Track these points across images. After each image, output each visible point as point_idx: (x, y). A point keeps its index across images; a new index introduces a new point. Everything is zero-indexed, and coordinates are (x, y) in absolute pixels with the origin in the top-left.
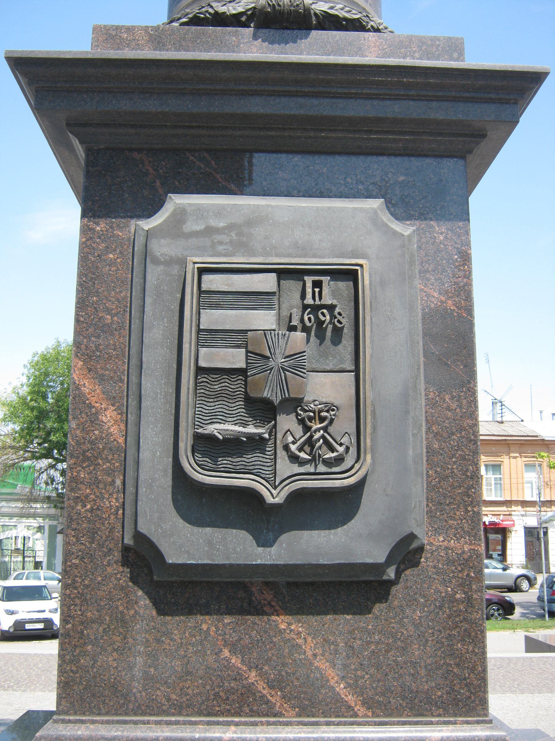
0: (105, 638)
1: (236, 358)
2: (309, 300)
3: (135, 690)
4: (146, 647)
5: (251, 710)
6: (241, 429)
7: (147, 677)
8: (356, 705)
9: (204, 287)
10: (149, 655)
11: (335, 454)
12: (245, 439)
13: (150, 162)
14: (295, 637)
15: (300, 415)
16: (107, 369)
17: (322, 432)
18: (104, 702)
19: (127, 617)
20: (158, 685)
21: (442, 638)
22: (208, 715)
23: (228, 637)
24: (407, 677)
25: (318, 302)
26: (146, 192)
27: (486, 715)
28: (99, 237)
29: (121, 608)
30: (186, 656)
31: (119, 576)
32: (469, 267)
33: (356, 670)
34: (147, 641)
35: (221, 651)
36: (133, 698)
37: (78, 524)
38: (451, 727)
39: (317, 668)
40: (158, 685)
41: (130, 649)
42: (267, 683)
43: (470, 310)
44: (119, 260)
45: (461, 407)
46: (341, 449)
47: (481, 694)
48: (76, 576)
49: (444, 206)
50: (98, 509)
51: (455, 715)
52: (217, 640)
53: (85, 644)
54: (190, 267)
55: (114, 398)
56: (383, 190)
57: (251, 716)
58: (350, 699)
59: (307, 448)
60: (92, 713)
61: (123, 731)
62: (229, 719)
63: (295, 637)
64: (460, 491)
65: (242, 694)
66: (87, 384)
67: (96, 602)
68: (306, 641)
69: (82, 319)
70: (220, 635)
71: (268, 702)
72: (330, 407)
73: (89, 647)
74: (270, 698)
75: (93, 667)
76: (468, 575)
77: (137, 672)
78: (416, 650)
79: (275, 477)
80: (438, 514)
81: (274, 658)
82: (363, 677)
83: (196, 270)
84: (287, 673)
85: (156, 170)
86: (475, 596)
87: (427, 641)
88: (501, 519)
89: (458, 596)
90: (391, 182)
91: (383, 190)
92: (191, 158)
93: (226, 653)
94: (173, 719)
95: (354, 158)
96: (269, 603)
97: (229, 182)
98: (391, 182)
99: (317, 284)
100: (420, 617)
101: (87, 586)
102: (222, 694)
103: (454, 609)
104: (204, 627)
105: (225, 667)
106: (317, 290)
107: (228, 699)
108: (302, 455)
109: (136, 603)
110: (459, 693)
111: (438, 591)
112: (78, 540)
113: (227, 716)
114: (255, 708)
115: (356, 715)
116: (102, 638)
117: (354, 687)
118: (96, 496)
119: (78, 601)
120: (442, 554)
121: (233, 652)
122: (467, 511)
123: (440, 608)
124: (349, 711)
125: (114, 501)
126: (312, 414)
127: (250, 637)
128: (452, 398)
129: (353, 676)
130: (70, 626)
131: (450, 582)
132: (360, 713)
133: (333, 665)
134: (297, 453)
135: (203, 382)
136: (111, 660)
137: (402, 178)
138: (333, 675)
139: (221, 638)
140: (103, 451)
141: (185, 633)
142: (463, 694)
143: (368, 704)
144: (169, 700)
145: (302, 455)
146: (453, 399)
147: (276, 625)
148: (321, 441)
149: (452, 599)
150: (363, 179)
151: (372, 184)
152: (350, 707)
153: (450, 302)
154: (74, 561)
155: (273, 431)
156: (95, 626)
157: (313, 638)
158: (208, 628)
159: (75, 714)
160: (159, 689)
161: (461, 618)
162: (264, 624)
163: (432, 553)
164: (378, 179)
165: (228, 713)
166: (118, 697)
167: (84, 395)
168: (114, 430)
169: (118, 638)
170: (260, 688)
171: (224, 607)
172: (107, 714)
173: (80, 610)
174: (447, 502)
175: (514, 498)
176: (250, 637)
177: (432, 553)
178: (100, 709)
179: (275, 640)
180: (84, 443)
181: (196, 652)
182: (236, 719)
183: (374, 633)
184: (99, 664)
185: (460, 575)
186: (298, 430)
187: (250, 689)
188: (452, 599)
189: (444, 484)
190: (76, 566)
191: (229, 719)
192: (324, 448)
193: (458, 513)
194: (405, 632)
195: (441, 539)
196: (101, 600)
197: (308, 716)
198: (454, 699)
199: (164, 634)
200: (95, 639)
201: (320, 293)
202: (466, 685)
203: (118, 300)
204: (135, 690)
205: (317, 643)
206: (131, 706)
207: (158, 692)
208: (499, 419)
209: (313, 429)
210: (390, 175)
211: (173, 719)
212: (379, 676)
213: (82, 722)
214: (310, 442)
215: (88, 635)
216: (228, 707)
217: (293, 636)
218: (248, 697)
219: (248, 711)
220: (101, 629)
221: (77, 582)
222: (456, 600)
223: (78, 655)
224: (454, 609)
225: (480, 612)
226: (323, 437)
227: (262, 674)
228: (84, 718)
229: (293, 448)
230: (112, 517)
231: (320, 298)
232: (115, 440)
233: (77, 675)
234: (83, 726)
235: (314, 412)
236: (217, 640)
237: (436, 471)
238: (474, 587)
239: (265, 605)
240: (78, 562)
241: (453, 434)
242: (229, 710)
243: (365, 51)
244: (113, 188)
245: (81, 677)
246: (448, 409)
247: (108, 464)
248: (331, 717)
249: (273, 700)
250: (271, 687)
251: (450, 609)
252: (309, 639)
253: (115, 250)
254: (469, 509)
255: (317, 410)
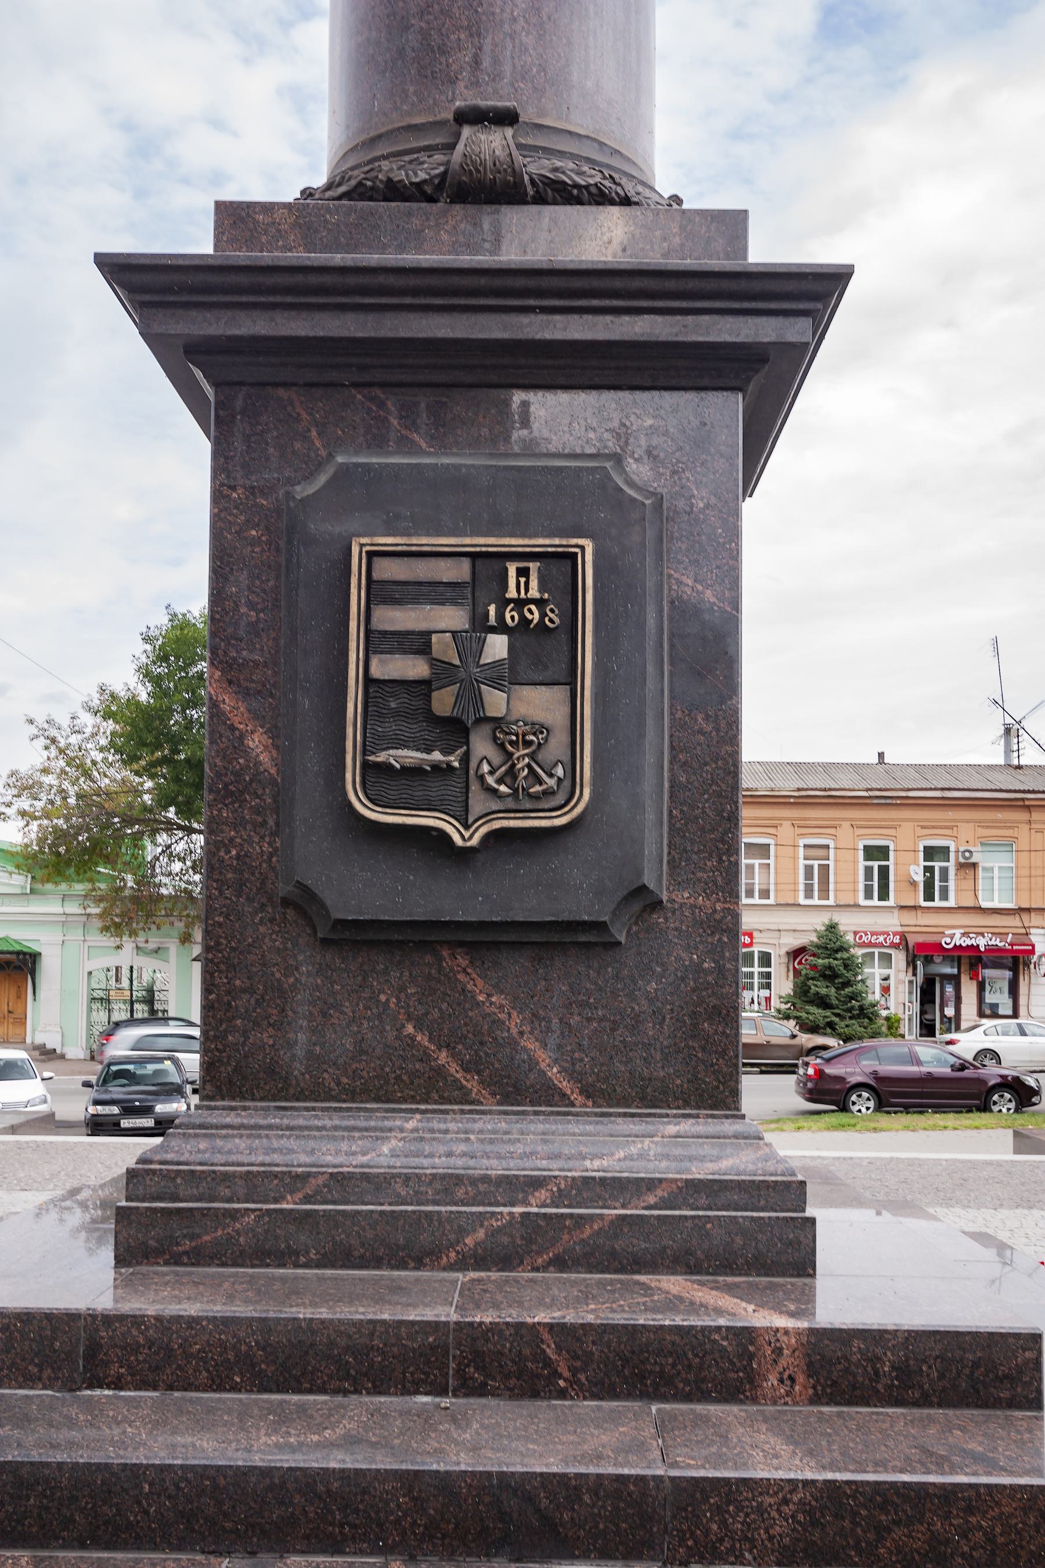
0: (258, 1010)
1: (415, 668)
2: (512, 593)
3: (296, 1073)
4: (309, 1021)
5: (441, 1097)
6: (424, 756)
7: (310, 1055)
8: (572, 1093)
9: (376, 576)
10: (313, 1031)
11: (544, 787)
12: (429, 768)
13: (302, 403)
14: (496, 1011)
15: (499, 739)
16: (253, 681)
17: (527, 760)
18: (258, 1087)
19: (286, 986)
20: (325, 1067)
21: (684, 1015)
22: (388, 1101)
23: (412, 1010)
24: (638, 1061)
25: (523, 595)
26: (297, 445)
27: (738, 1109)
28: (237, 507)
29: (278, 975)
30: (360, 1032)
31: (274, 936)
32: (737, 544)
33: (573, 1051)
34: (311, 1013)
35: (403, 1026)
36: (294, 1082)
37: (221, 873)
38: (691, 1121)
39: (525, 1049)
40: (325, 1067)
41: (289, 1024)
42: (462, 1066)
43: (736, 604)
44: (264, 538)
45: (718, 730)
46: (551, 782)
47: (732, 1084)
48: (221, 937)
49: (706, 460)
50: (246, 855)
51: (699, 1108)
52: (399, 1013)
53: (233, 1017)
54: (355, 550)
55: (264, 717)
56: (623, 440)
57: (442, 1104)
58: (565, 1085)
59: (508, 780)
60: (244, 1098)
61: (282, 1119)
62: (414, 1106)
63: (496, 1011)
64: (712, 836)
65: (429, 1078)
66: (227, 700)
67: (246, 967)
68: (510, 1016)
69: (217, 616)
70: (403, 1007)
71: (462, 1087)
72: (539, 728)
73: (239, 1022)
74: (464, 1083)
75: (244, 1044)
76: (720, 940)
77: (300, 1051)
78: (650, 1029)
79: (467, 815)
80: (683, 864)
81: (470, 1035)
82: (582, 1060)
83: (364, 554)
84: (486, 1054)
85: (311, 414)
86: (728, 966)
87: (664, 1018)
88: (1009, 941)
89: (706, 965)
90: (634, 428)
91: (623, 440)
92: (359, 396)
93: (410, 1029)
94: (344, 1105)
95: (583, 395)
96: (464, 970)
97: (410, 430)
98: (634, 428)
99: (523, 572)
100: (656, 990)
101: (233, 949)
102: (405, 1078)
103: (701, 980)
104: (383, 998)
105: (408, 1045)
106: (523, 580)
107: (412, 1083)
108: (503, 788)
109: (297, 969)
110: (705, 1082)
111: (679, 959)
112: (221, 893)
113: (411, 1103)
114: (445, 1095)
115: (573, 1105)
116: (254, 1011)
117: (572, 1074)
118: (243, 840)
119: (223, 967)
120: (687, 914)
121: (418, 1027)
122: (720, 861)
123: (683, 979)
124: (564, 1099)
125: (266, 845)
126: (514, 738)
127: (440, 1009)
128: (707, 717)
129: (569, 1059)
130: (212, 997)
131: (697, 948)
132: (577, 1103)
133: (544, 1046)
134: (496, 786)
135: (376, 697)
136: (266, 1037)
137: (650, 422)
138: (544, 1058)
139: (402, 1011)
140: (250, 784)
141: (358, 1005)
142: (709, 1083)
143: (588, 1092)
144: (338, 1084)
145: (503, 788)
146: (707, 719)
147: (473, 997)
148: (526, 771)
149: (698, 969)
150: (595, 425)
151: (607, 430)
152: (564, 1095)
153: (708, 592)
154: (217, 919)
155: (465, 759)
156: (246, 996)
157: (519, 1013)
158: (387, 1000)
159: (223, 1099)
160: (326, 1071)
161: (710, 991)
162: (457, 995)
163: (674, 913)
164: (615, 424)
165: (413, 1100)
166: (275, 1080)
167: (224, 713)
168: (264, 758)
169: (275, 1011)
170: (452, 1071)
171: (408, 974)
172: (262, 1099)
173: (227, 977)
174: (696, 850)
175: (1033, 906)
176: (440, 1009)
177: (674, 913)
178: (253, 1094)
179: (470, 1014)
180: (226, 774)
181: (372, 1027)
182: (423, 1107)
183: (596, 1008)
184: (251, 1041)
185: (710, 939)
186: (496, 758)
187: (440, 1072)
188: (698, 969)
189: (692, 827)
190: (220, 925)
191: (414, 1106)
192: (531, 780)
193: (709, 863)
194: (636, 1008)
195: (686, 895)
196: (252, 965)
197: (512, 1105)
198: (697, 1089)
199: (332, 1006)
200: (246, 1012)
201: (527, 584)
202: (713, 1073)
203: (264, 591)
204: (296, 1073)
205: (524, 1018)
206: (292, 1091)
207: (326, 1075)
208: (1015, 762)
209: (516, 756)
210: (633, 418)
211: (344, 1105)
212: (601, 1060)
213: (232, 1109)
214: (512, 772)
215: (237, 1007)
216: (412, 1093)
217: (493, 1009)
218: (438, 1081)
219: (437, 1098)
220: (253, 1001)
221: (221, 944)
222: (703, 970)
223: (225, 1031)
224: (701, 980)
225: (734, 985)
226: (529, 766)
227: (454, 1055)
228: (234, 1104)
229: (490, 780)
230: (264, 865)
231: (527, 590)
232: (266, 770)
233: (224, 1054)
234: (233, 1113)
235: (517, 735)
236: (399, 1013)
237: (682, 811)
238: (727, 954)
239: (459, 972)
240: (222, 919)
241: (706, 764)
242: (413, 1097)
243: (601, 239)
244: (253, 439)
245: (229, 1057)
246: (701, 732)
247: (258, 801)
248: (540, 1105)
249: (469, 1086)
250: (466, 1070)
251: (695, 980)
252: (514, 1014)
253: (258, 525)
254: (724, 858)
255: (520, 732)
